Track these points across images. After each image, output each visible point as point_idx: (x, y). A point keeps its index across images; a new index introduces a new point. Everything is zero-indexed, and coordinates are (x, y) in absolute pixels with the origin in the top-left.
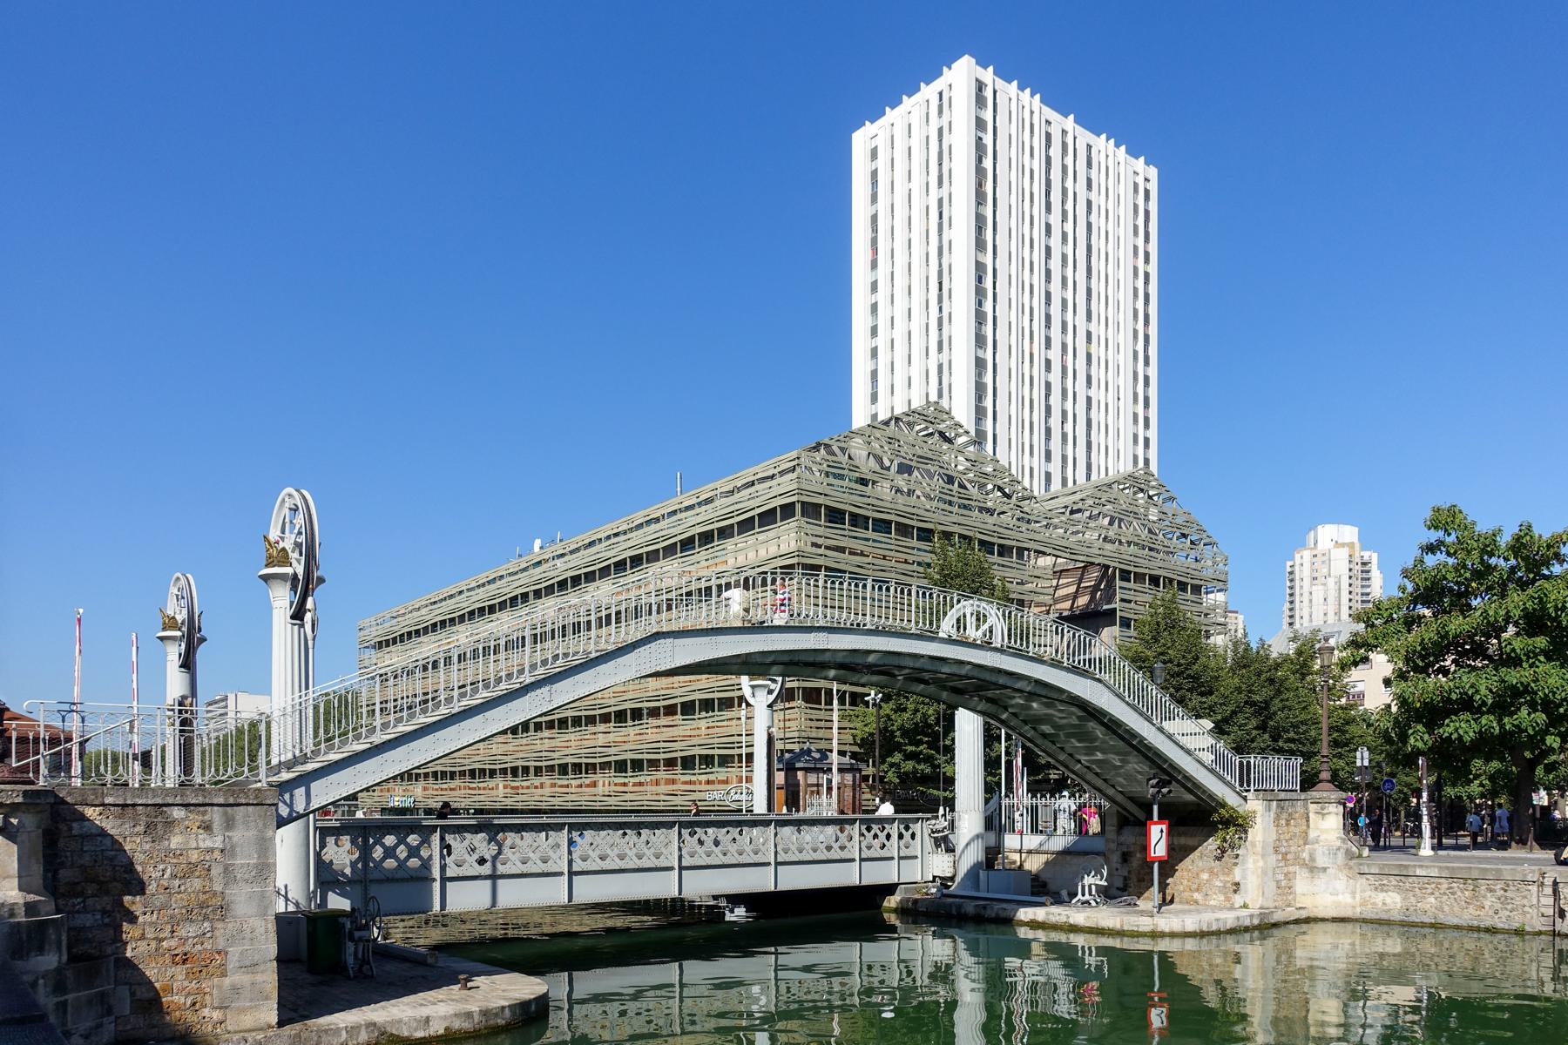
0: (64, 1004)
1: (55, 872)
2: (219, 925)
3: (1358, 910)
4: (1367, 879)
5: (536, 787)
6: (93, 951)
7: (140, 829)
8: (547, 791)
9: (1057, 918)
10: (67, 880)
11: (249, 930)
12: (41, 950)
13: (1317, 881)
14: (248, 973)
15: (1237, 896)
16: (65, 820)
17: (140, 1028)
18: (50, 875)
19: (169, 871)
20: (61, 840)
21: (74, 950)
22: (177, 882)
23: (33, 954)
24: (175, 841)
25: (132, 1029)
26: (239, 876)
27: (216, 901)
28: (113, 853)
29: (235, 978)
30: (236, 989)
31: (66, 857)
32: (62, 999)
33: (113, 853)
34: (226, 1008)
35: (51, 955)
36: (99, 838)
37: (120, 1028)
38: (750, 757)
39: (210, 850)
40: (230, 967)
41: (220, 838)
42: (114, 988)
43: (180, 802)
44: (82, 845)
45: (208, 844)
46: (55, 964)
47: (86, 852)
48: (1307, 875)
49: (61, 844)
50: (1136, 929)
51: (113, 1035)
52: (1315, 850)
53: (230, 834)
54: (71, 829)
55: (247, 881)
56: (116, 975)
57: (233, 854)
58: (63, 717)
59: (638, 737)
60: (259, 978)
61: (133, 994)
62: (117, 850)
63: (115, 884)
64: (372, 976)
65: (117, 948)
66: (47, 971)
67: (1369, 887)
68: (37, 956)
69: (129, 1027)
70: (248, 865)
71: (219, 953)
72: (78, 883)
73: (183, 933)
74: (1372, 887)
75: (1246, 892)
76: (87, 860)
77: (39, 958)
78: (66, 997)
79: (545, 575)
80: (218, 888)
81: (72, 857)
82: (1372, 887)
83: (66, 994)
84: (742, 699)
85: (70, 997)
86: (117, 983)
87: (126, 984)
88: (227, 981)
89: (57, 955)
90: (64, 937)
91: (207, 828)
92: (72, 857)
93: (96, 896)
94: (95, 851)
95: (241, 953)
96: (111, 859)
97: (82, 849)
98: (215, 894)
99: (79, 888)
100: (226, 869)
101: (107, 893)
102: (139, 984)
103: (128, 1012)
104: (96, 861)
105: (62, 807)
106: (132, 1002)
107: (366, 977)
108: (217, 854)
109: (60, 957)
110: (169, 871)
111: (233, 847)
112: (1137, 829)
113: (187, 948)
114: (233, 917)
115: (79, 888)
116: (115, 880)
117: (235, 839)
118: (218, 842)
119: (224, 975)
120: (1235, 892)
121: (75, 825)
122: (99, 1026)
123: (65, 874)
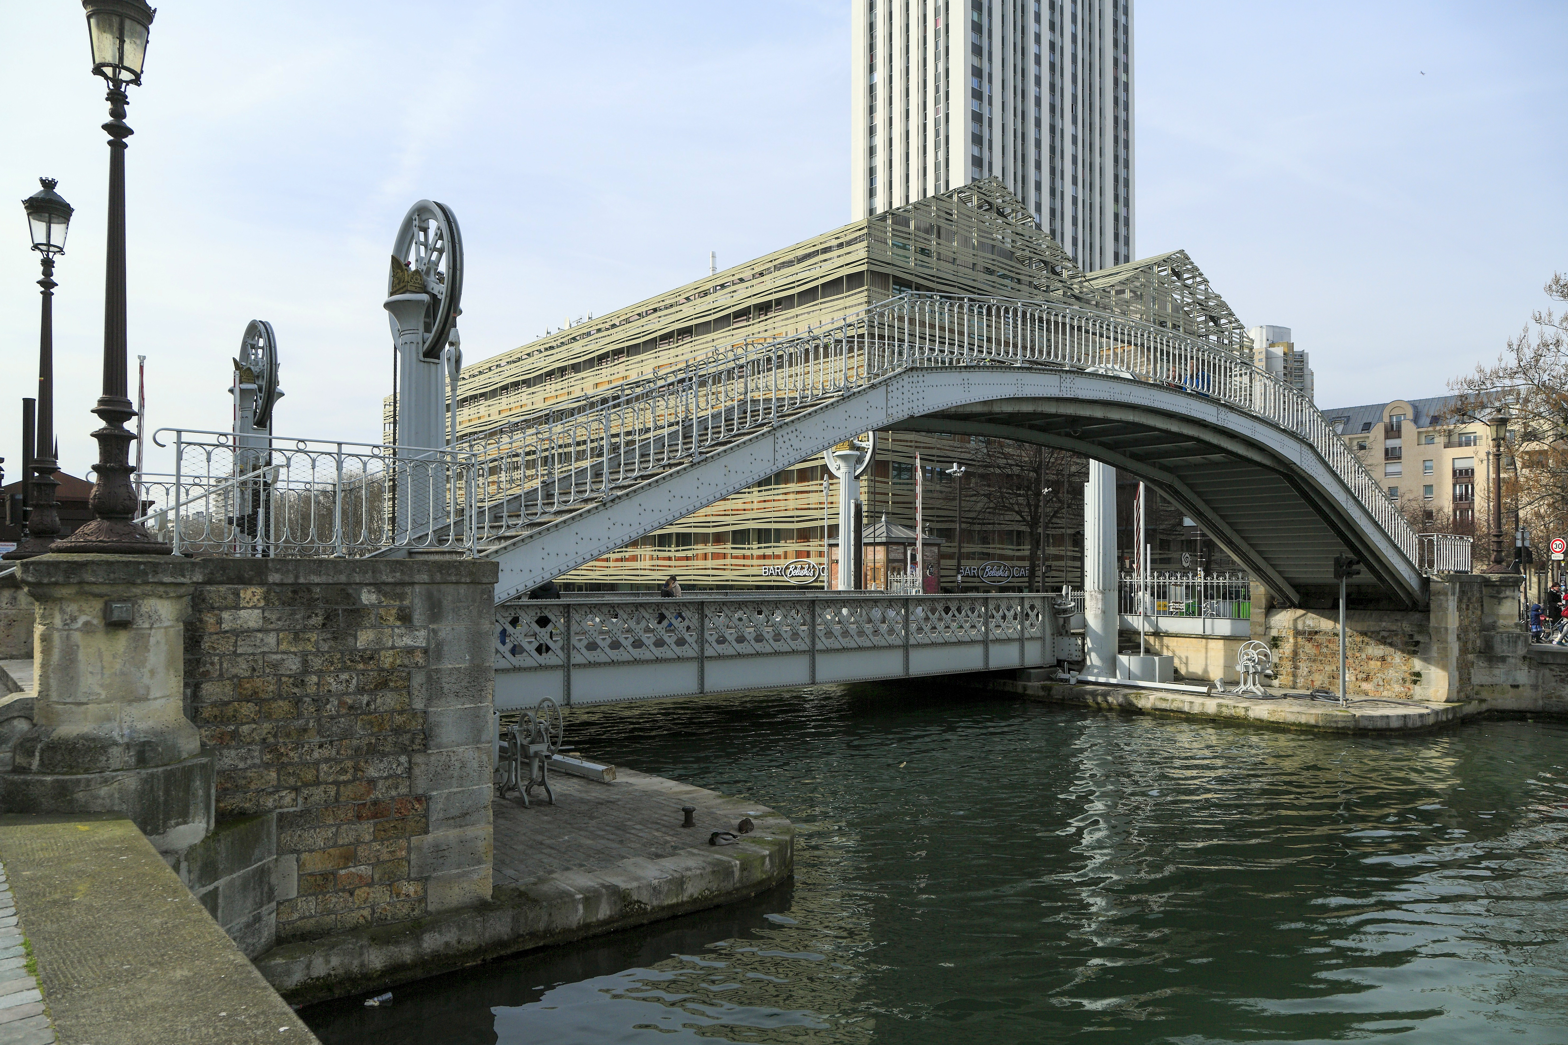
0: (215, 892)
1: (197, 687)
2: (419, 759)
3: (1540, 703)
4: (1551, 670)
5: (778, 557)
6: (247, 805)
7: (319, 620)
8: (647, 563)
9: (1233, 712)
10: (214, 698)
11: (458, 765)
12: (184, 817)
13: (1496, 672)
14: (456, 827)
15: (1417, 687)
16: (213, 608)
17: (311, 916)
18: (189, 691)
19: (354, 681)
20: (206, 638)
21: (222, 805)
22: (365, 699)
23: (173, 822)
24: (364, 638)
25: (301, 918)
26: (446, 686)
27: (416, 725)
28: (279, 657)
29: (439, 834)
30: (439, 851)
31: (212, 664)
32: (211, 887)
33: (279, 657)
34: (427, 879)
35: (197, 820)
36: (260, 635)
37: (284, 918)
38: (833, 530)
39: (410, 651)
40: (433, 818)
41: (423, 633)
42: (276, 860)
43: (372, 581)
44: (235, 645)
45: (407, 641)
46: (202, 835)
47: (241, 654)
48: (1486, 664)
49: (205, 645)
50: (1334, 725)
51: (273, 930)
52: (1492, 637)
53: (435, 626)
54: (220, 622)
55: (457, 694)
56: (279, 839)
57: (439, 656)
58: (209, 454)
59: (763, 505)
60: (470, 832)
61: (300, 865)
62: (283, 653)
63: (281, 703)
64: (550, 803)
65: (281, 797)
66: (192, 848)
67: (1553, 679)
68: (178, 824)
69: (296, 916)
70: (458, 670)
71: (418, 799)
72: (228, 703)
73: (372, 772)
74: (1558, 678)
75: (1429, 683)
76: (242, 668)
77: (182, 827)
78: (216, 884)
79: (644, 329)
80: (419, 705)
81: (221, 664)
82: (1558, 678)
83: (216, 879)
84: (825, 469)
85: (221, 883)
86: (281, 852)
87: (293, 851)
88: (430, 838)
89: (204, 821)
90: (213, 791)
91: (405, 618)
92: (221, 664)
93: (254, 721)
94: (253, 654)
95: (448, 798)
96: (275, 666)
97: (235, 652)
98: (415, 715)
99: (229, 711)
100: (429, 678)
101: (268, 717)
102: (311, 851)
103: (294, 894)
104: (254, 670)
105: (208, 588)
106: (300, 877)
107: (540, 803)
108: (419, 658)
109: (208, 823)
110: (354, 681)
111: (439, 646)
112: (1417, 616)
113: (377, 794)
114: (439, 746)
115: (229, 711)
116: (280, 697)
117: (442, 635)
118: (419, 638)
119: (426, 832)
120: (1415, 682)
121: (226, 615)
122: (258, 919)
123: (211, 690)
